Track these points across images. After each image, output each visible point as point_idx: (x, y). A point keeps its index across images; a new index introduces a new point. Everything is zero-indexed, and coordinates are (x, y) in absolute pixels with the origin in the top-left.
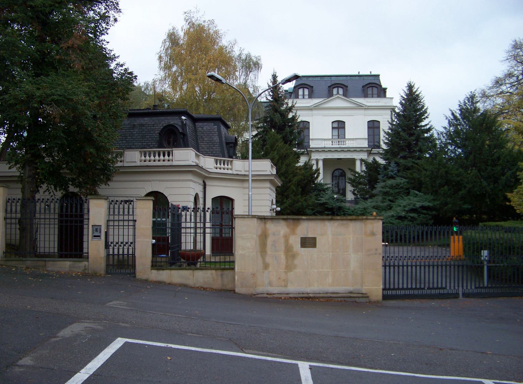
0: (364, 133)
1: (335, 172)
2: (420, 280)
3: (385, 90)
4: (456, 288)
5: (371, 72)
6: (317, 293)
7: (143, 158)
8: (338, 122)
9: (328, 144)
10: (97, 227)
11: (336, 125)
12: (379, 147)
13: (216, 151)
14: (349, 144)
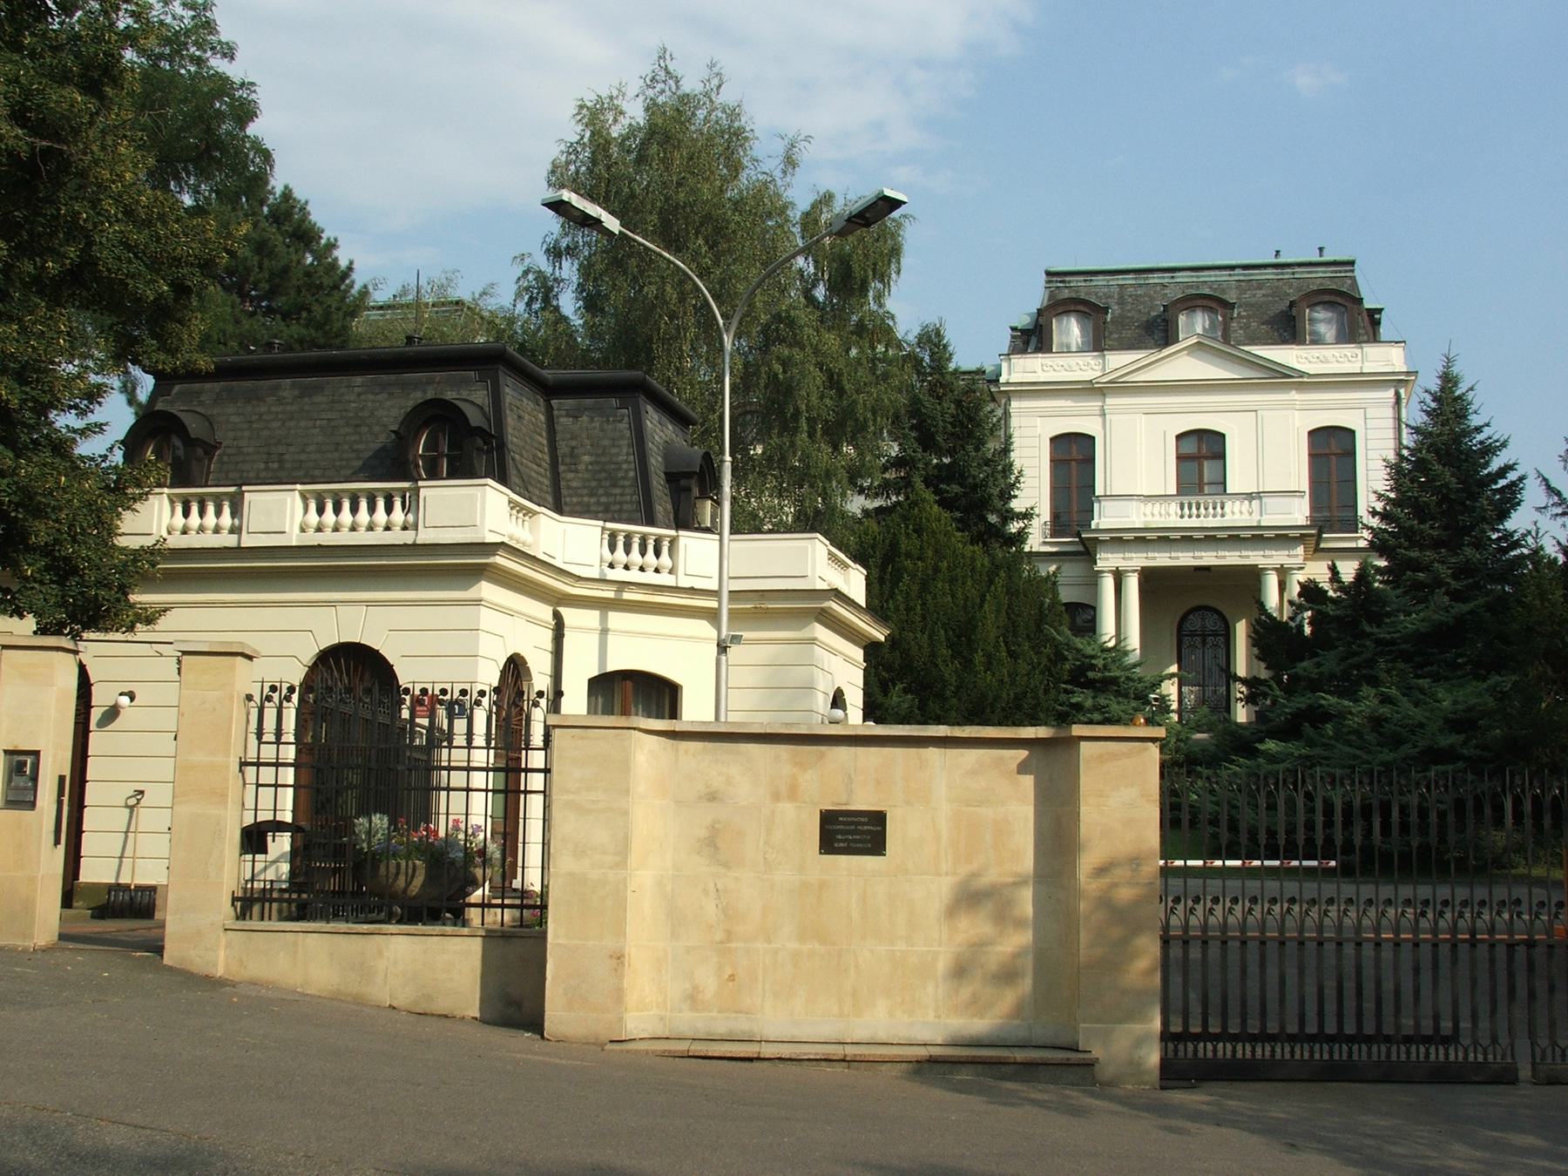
0: (1295, 470)
1: (1191, 617)
2: (1244, 1004)
3: (1374, 317)
4: (1504, 1041)
5: (1321, 249)
6: (1039, 1043)
7: (313, 518)
8: (1200, 433)
9: (1169, 516)
10: (22, 758)
11: (1190, 447)
12: (1352, 524)
13: (621, 503)
14: (1237, 515)
